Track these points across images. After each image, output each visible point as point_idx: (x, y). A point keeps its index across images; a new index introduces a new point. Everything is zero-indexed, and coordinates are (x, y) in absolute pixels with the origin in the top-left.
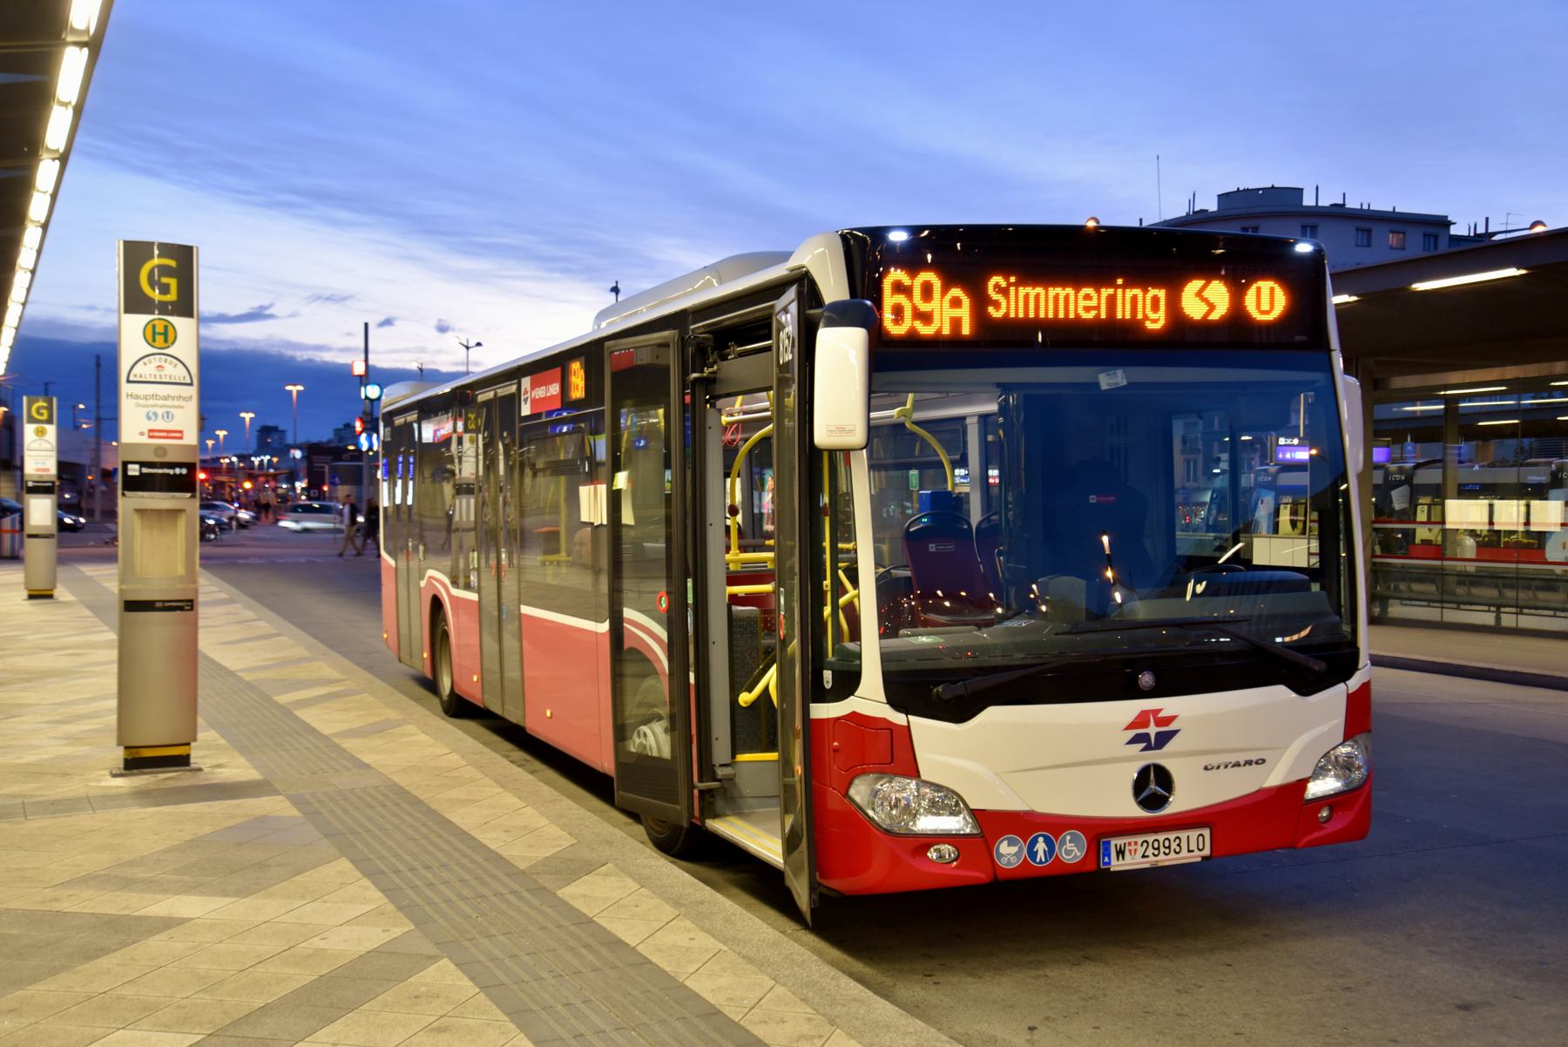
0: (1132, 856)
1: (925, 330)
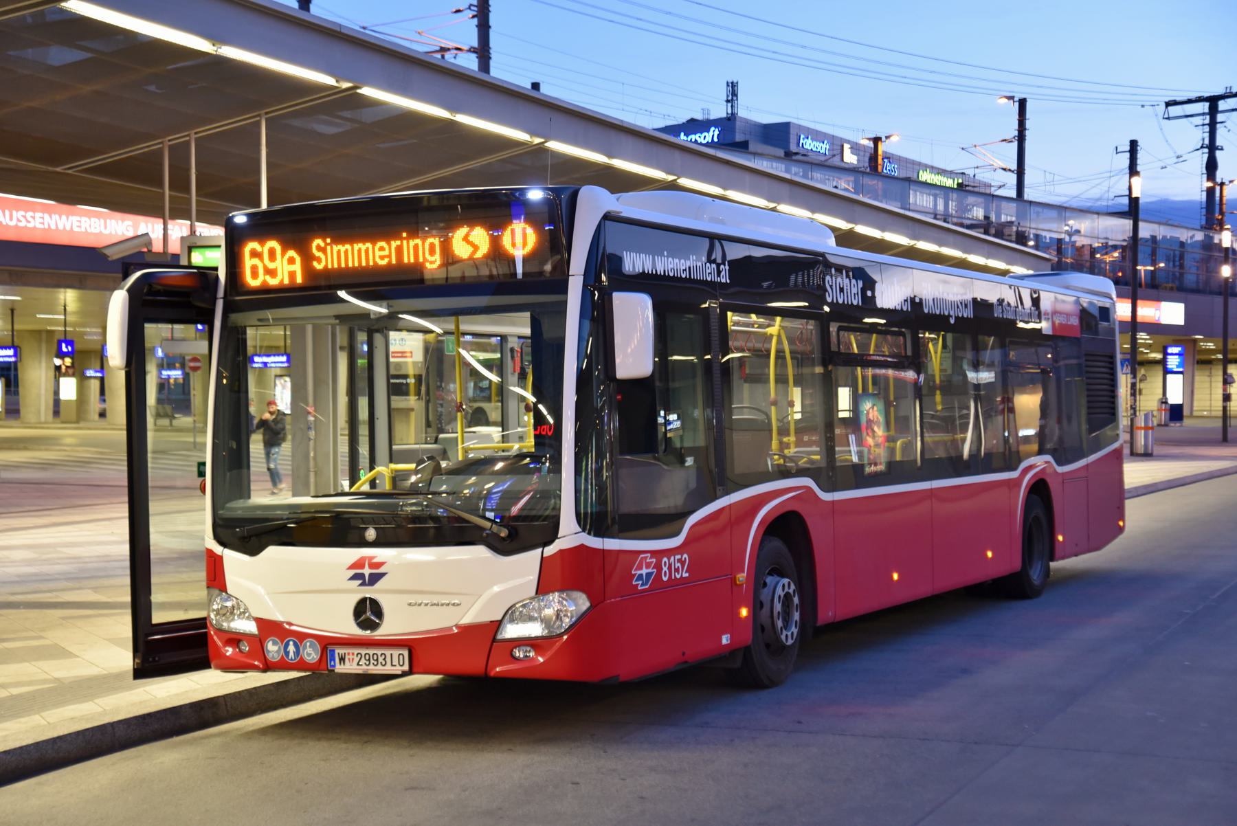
1: (273, 282)
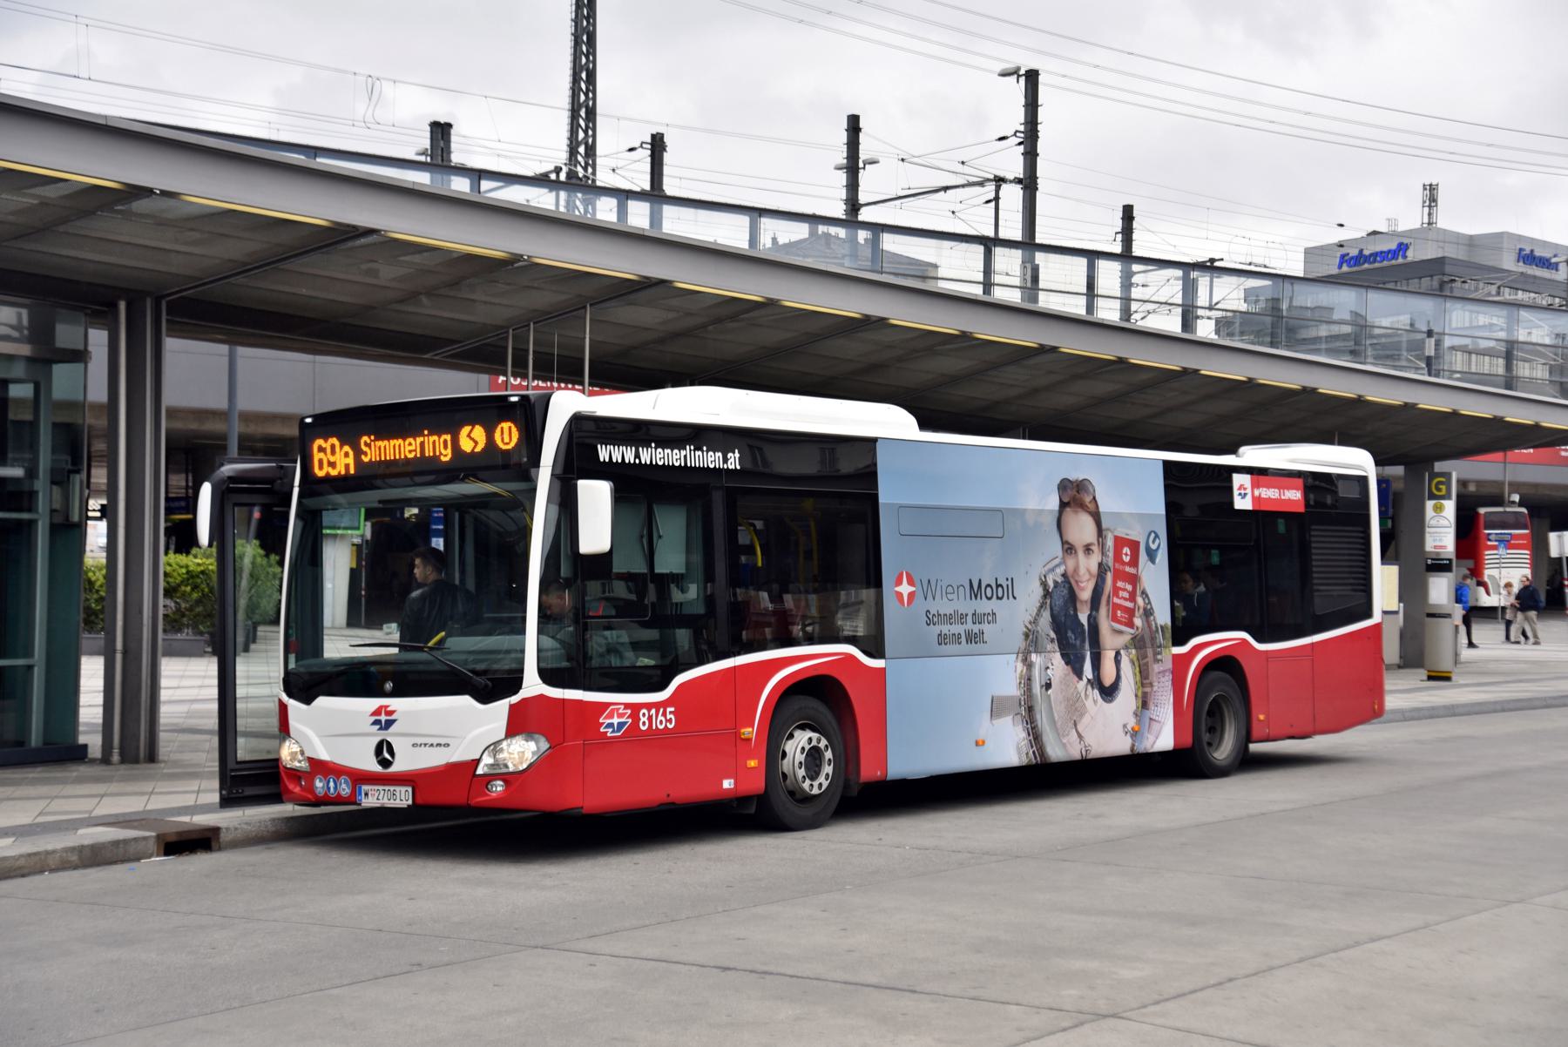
0: (374, 797)
1: (334, 473)
